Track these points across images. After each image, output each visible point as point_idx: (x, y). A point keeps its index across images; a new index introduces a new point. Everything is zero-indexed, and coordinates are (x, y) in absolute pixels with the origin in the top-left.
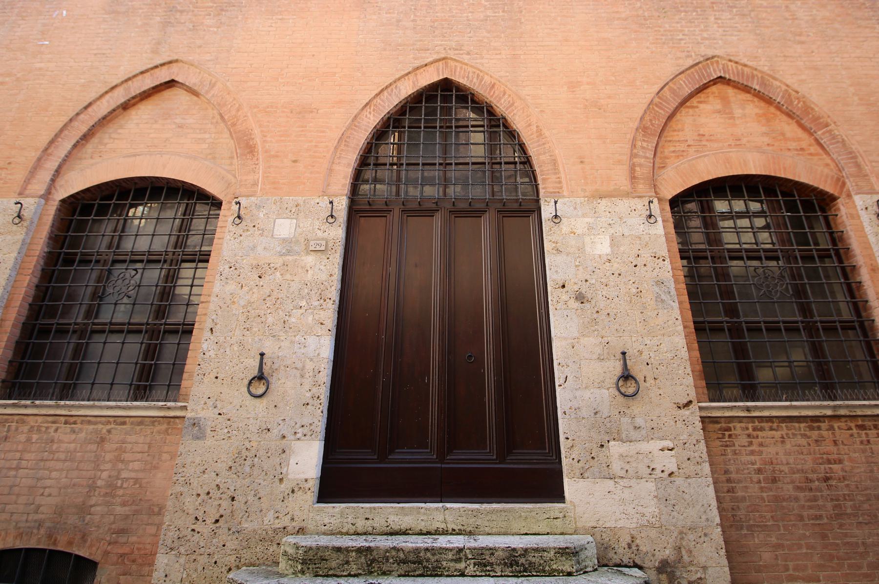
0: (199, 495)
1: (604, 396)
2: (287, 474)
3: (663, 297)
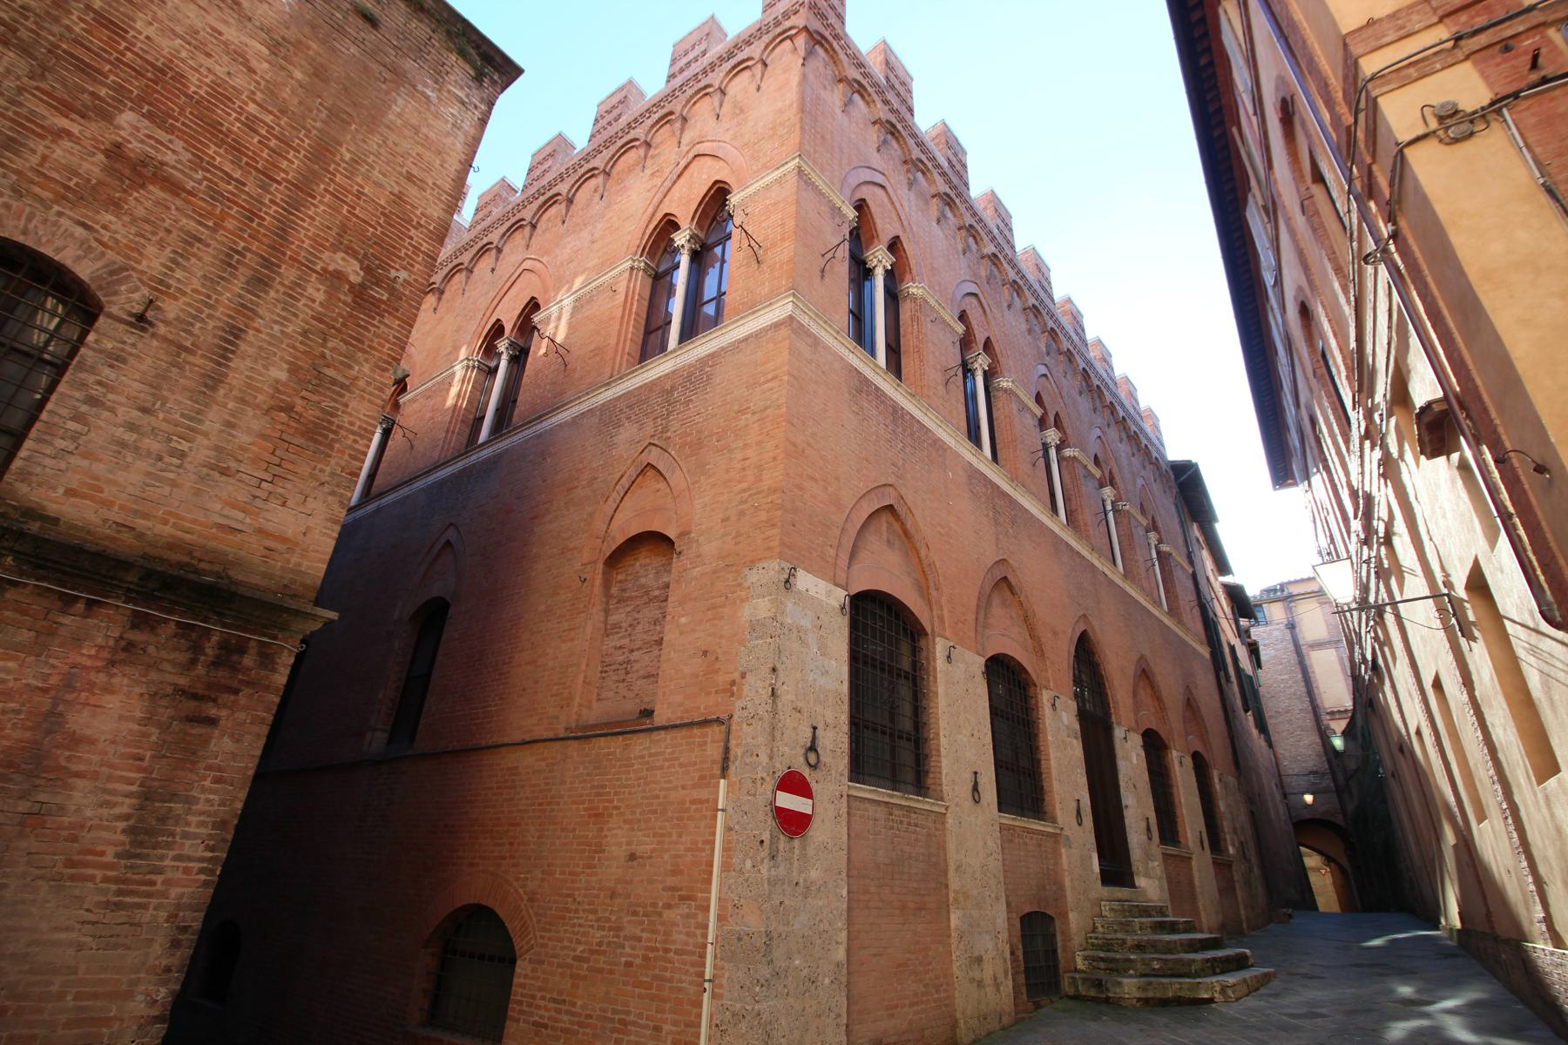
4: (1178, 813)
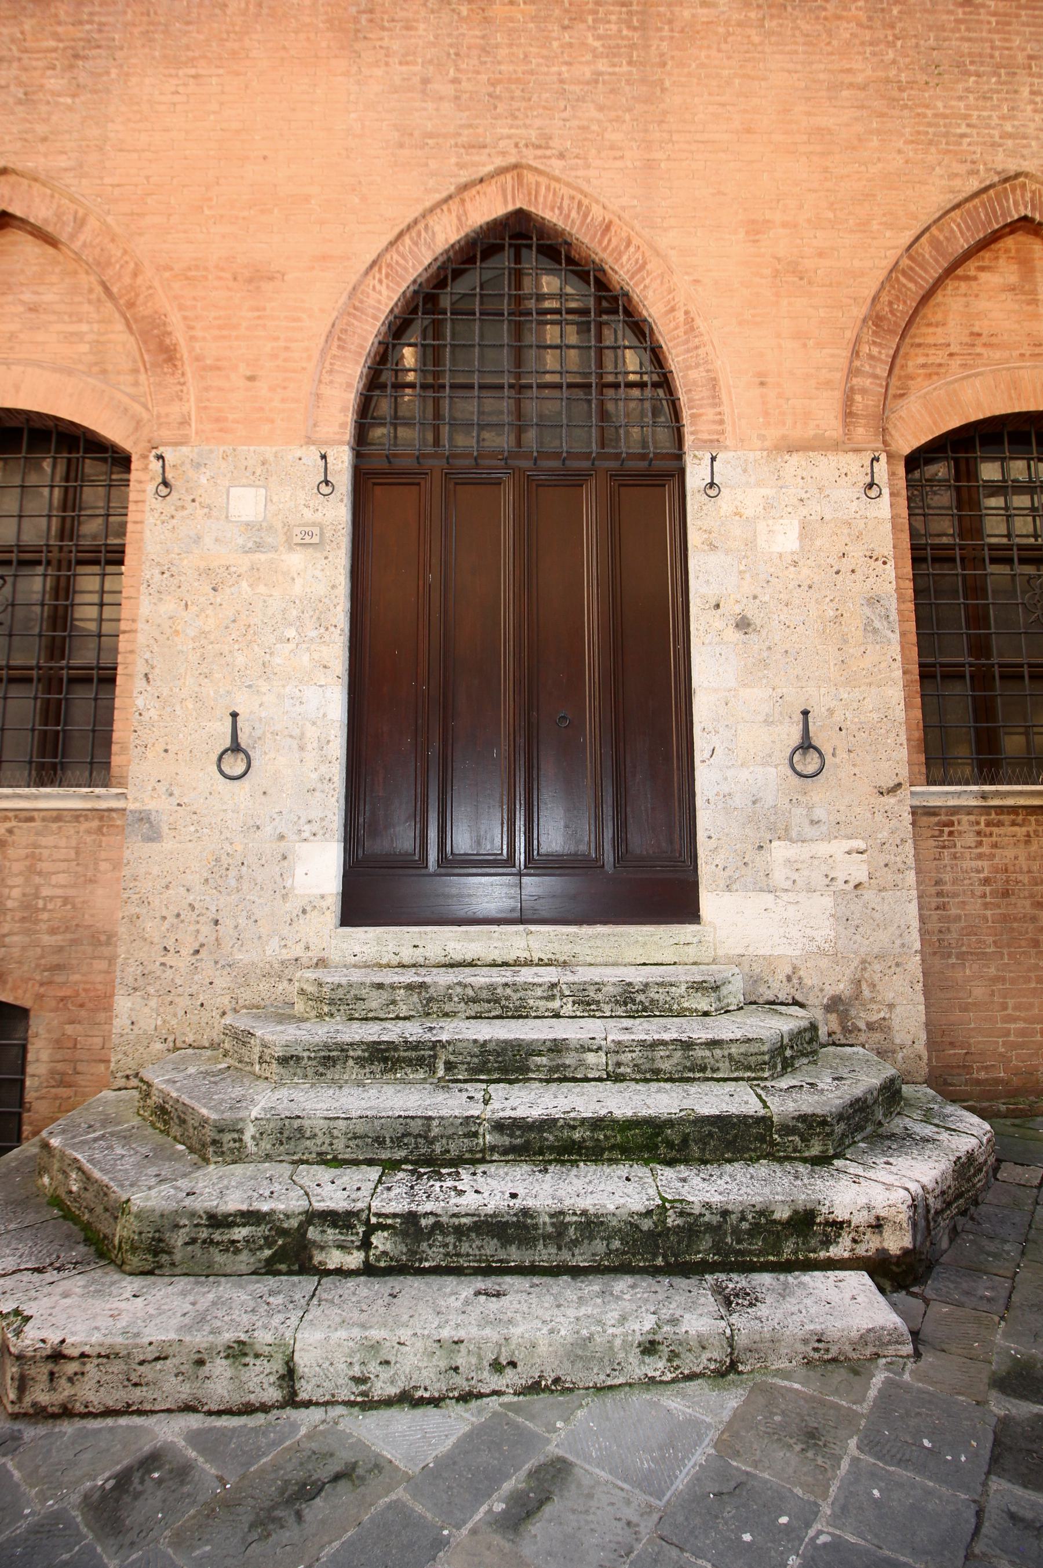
0: (164, 918)
2: (293, 888)
3: (877, 624)
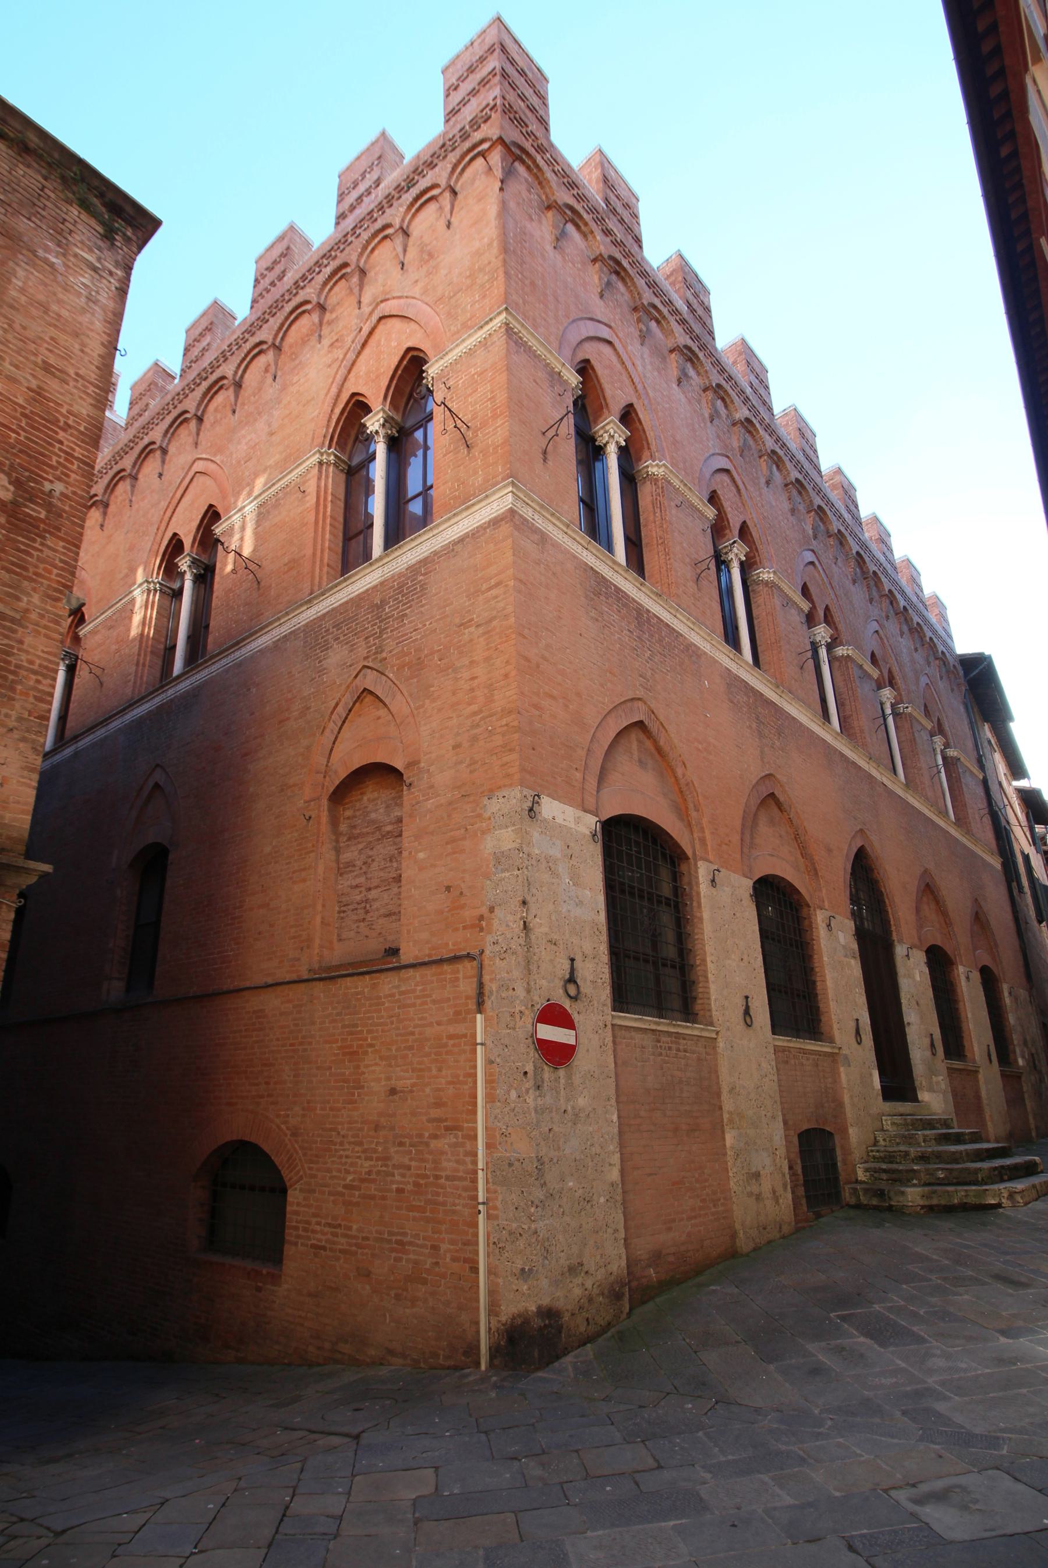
1: (928, 1053)
4: (964, 1026)
